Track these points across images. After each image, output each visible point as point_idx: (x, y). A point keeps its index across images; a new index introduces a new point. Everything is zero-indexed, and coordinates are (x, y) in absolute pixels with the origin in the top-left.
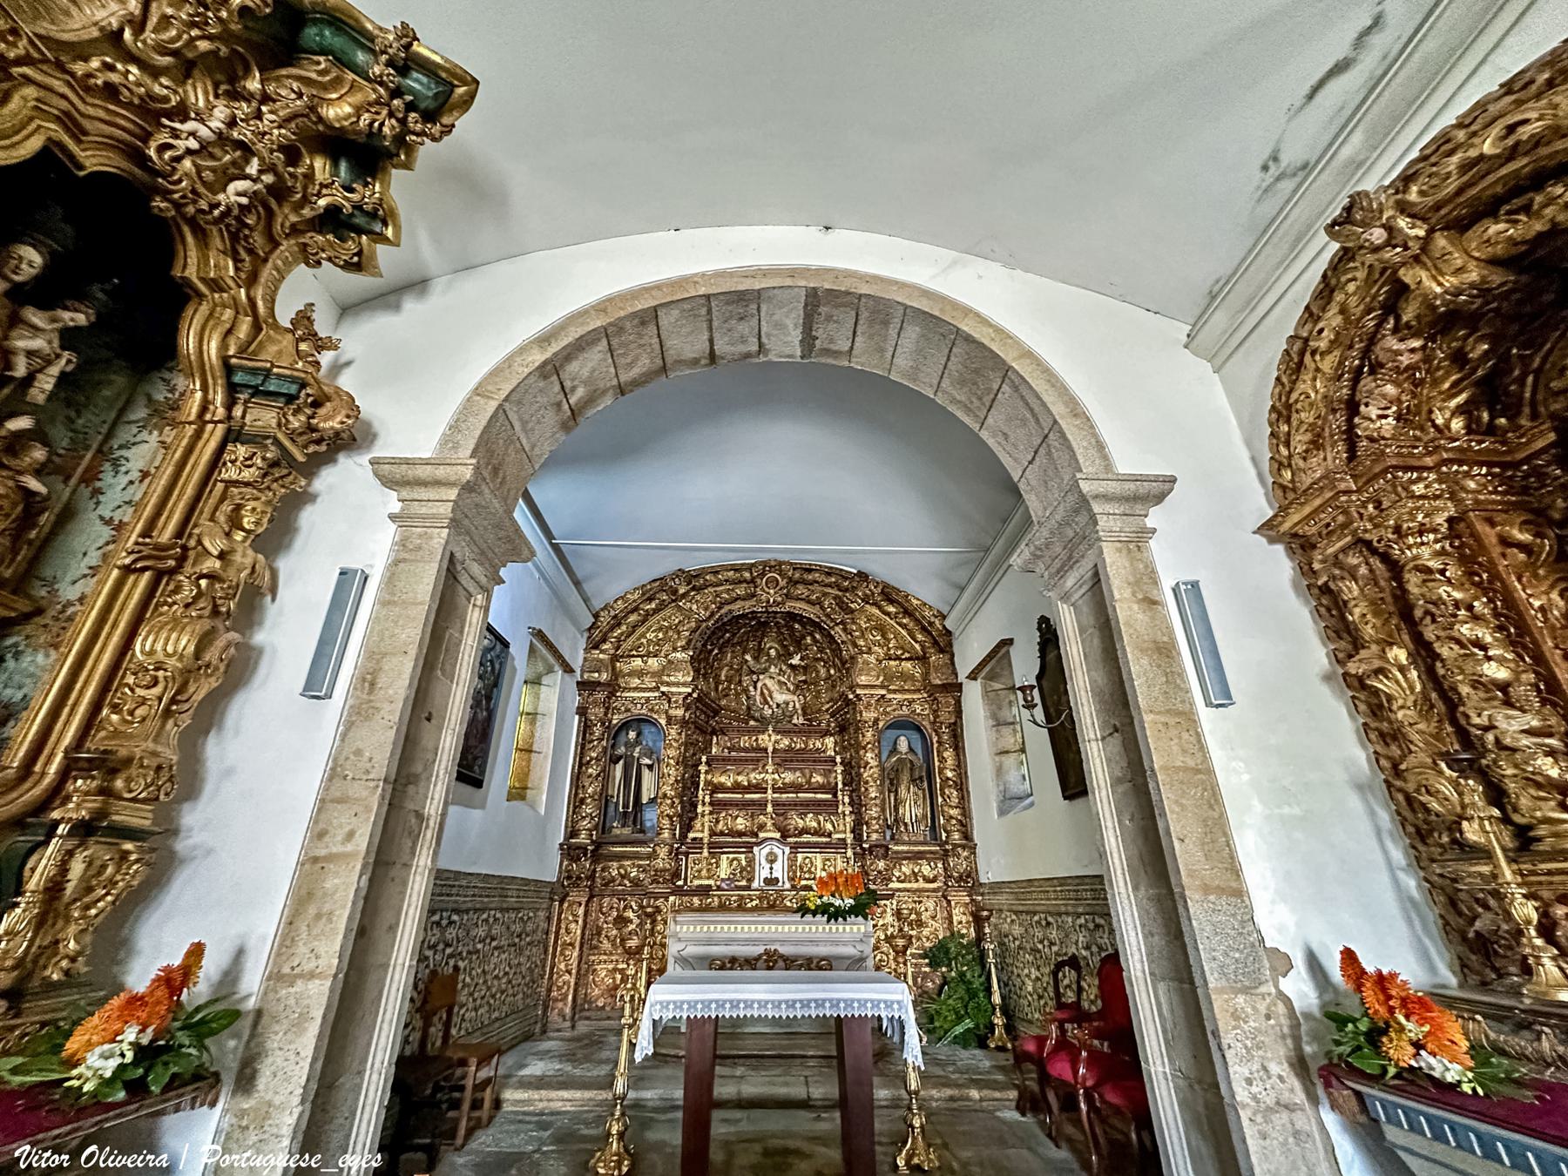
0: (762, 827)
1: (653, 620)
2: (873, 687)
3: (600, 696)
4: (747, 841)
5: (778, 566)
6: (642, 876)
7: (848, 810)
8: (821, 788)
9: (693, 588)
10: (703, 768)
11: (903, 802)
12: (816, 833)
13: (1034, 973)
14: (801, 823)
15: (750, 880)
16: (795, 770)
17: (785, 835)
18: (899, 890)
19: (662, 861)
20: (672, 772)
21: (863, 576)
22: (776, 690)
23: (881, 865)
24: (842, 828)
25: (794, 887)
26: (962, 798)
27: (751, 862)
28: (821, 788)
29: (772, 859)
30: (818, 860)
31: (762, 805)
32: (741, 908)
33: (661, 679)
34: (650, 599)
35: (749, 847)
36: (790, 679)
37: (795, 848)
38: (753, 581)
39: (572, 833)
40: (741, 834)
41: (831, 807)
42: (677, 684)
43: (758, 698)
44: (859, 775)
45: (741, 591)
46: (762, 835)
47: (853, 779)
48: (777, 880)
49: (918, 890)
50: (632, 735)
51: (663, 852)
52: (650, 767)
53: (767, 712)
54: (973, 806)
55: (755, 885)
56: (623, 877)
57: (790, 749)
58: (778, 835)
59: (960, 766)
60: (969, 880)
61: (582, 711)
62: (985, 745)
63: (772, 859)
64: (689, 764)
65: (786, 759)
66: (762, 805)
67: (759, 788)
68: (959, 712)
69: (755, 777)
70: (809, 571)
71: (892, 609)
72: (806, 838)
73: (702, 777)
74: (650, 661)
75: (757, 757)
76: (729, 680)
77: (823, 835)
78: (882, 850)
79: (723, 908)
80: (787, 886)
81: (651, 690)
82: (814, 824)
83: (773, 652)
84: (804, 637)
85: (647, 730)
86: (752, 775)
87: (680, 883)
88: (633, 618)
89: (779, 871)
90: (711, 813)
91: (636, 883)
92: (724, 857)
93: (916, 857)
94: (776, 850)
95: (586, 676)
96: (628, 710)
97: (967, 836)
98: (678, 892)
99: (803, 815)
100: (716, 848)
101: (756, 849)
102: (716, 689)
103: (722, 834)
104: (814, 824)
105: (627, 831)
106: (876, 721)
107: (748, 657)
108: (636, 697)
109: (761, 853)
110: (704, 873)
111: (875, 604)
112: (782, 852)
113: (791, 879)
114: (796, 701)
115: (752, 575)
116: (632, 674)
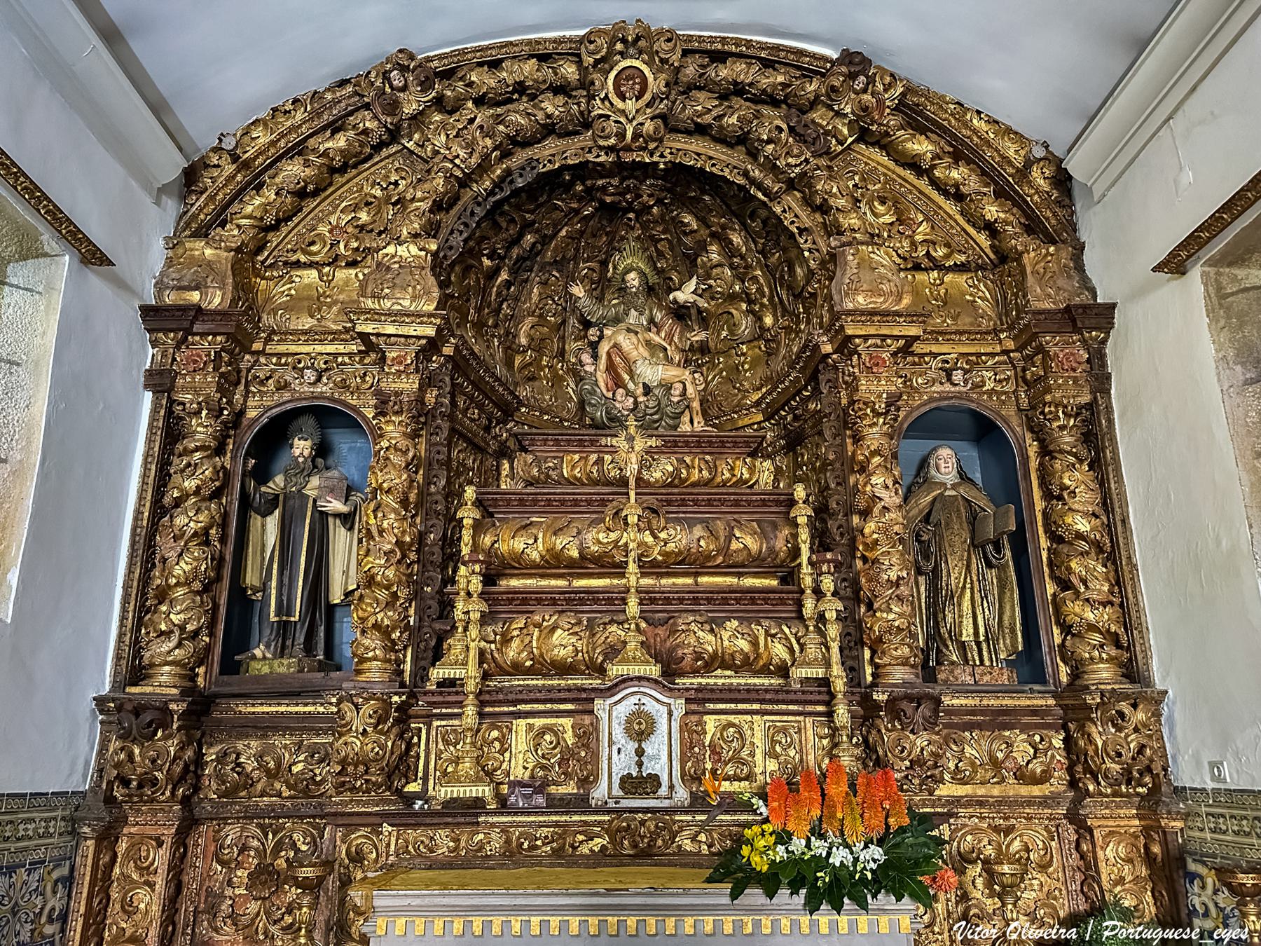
0: (614, 651)
1: (347, 189)
2: (886, 315)
3: (206, 346)
4: (578, 687)
5: (637, 39)
6: (320, 771)
7: (832, 607)
8: (755, 564)
9: (438, 103)
10: (468, 514)
11: (953, 598)
12: (747, 664)
13: (985, 842)
14: (709, 643)
15: (587, 782)
16: (691, 524)
17: (671, 670)
18: (957, 801)
19: (361, 736)
20: (392, 524)
21: (855, 62)
22: (642, 358)
23: (920, 742)
24: (813, 651)
25: (699, 802)
26: (1117, 582)
27: (588, 737)
28: (755, 564)
29: (640, 729)
30: (757, 729)
31: (615, 601)
32: (563, 856)
33: (363, 303)
34: (335, 127)
35: (583, 701)
36: (668, 335)
37: (699, 700)
38: (585, 84)
39: (134, 669)
40: (564, 669)
41: (785, 601)
42: (397, 316)
43: (601, 378)
44: (853, 536)
45: (551, 106)
46: (615, 670)
47: (835, 533)
48: (655, 780)
49: (1001, 802)
50: (302, 447)
51: (360, 719)
52: (347, 520)
53: (623, 403)
54: (1146, 602)
55: (599, 793)
56: (272, 775)
57: (675, 481)
58: (655, 671)
59: (1109, 505)
60: (1150, 784)
61: (161, 381)
62: (1222, 433)
63: (640, 729)
64: (431, 507)
65: (670, 501)
66: (615, 601)
67: (607, 564)
68: (1100, 380)
69: (597, 539)
70: (719, 57)
71: (921, 147)
72: (722, 678)
73: (467, 536)
74: (341, 274)
75: (602, 497)
76: (538, 346)
77: (765, 671)
78: (916, 705)
79: (514, 855)
80: (682, 794)
81: (336, 337)
82: (743, 644)
83: (633, 279)
84: (702, 247)
85: (343, 442)
86: (589, 537)
87: (413, 787)
88: (293, 170)
89: (661, 757)
90: (485, 619)
91: (306, 787)
92: (522, 723)
93: (999, 721)
94: (651, 706)
95: (170, 298)
96: (283, 387)
97: (1132, 671)
98: (408, 814)
99: (714, 625)
100: (495, 703)
101: (600, 706)
102: (509, 363)
103: (518, 669)
104: (743, 644)
105: (285, 667)
106: (893, 401)
107: (578, 291)
108: (302, 359)
109: (614, 714)
110: (467, 766)
111: (884, 143)
112: (665, 710)
113: (692, 778)
114: (689, 382)
115: (574, 66)
116: (293, 305)
